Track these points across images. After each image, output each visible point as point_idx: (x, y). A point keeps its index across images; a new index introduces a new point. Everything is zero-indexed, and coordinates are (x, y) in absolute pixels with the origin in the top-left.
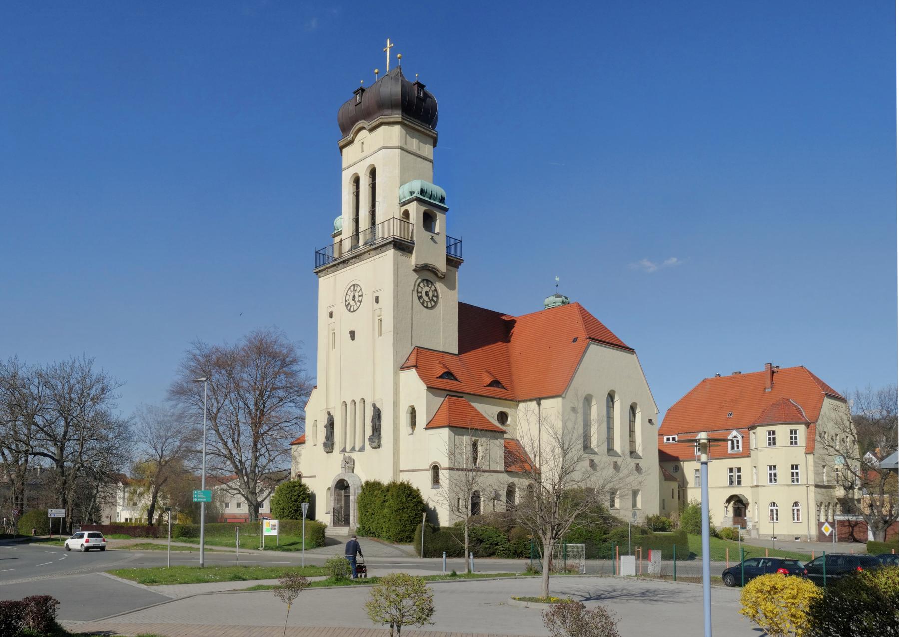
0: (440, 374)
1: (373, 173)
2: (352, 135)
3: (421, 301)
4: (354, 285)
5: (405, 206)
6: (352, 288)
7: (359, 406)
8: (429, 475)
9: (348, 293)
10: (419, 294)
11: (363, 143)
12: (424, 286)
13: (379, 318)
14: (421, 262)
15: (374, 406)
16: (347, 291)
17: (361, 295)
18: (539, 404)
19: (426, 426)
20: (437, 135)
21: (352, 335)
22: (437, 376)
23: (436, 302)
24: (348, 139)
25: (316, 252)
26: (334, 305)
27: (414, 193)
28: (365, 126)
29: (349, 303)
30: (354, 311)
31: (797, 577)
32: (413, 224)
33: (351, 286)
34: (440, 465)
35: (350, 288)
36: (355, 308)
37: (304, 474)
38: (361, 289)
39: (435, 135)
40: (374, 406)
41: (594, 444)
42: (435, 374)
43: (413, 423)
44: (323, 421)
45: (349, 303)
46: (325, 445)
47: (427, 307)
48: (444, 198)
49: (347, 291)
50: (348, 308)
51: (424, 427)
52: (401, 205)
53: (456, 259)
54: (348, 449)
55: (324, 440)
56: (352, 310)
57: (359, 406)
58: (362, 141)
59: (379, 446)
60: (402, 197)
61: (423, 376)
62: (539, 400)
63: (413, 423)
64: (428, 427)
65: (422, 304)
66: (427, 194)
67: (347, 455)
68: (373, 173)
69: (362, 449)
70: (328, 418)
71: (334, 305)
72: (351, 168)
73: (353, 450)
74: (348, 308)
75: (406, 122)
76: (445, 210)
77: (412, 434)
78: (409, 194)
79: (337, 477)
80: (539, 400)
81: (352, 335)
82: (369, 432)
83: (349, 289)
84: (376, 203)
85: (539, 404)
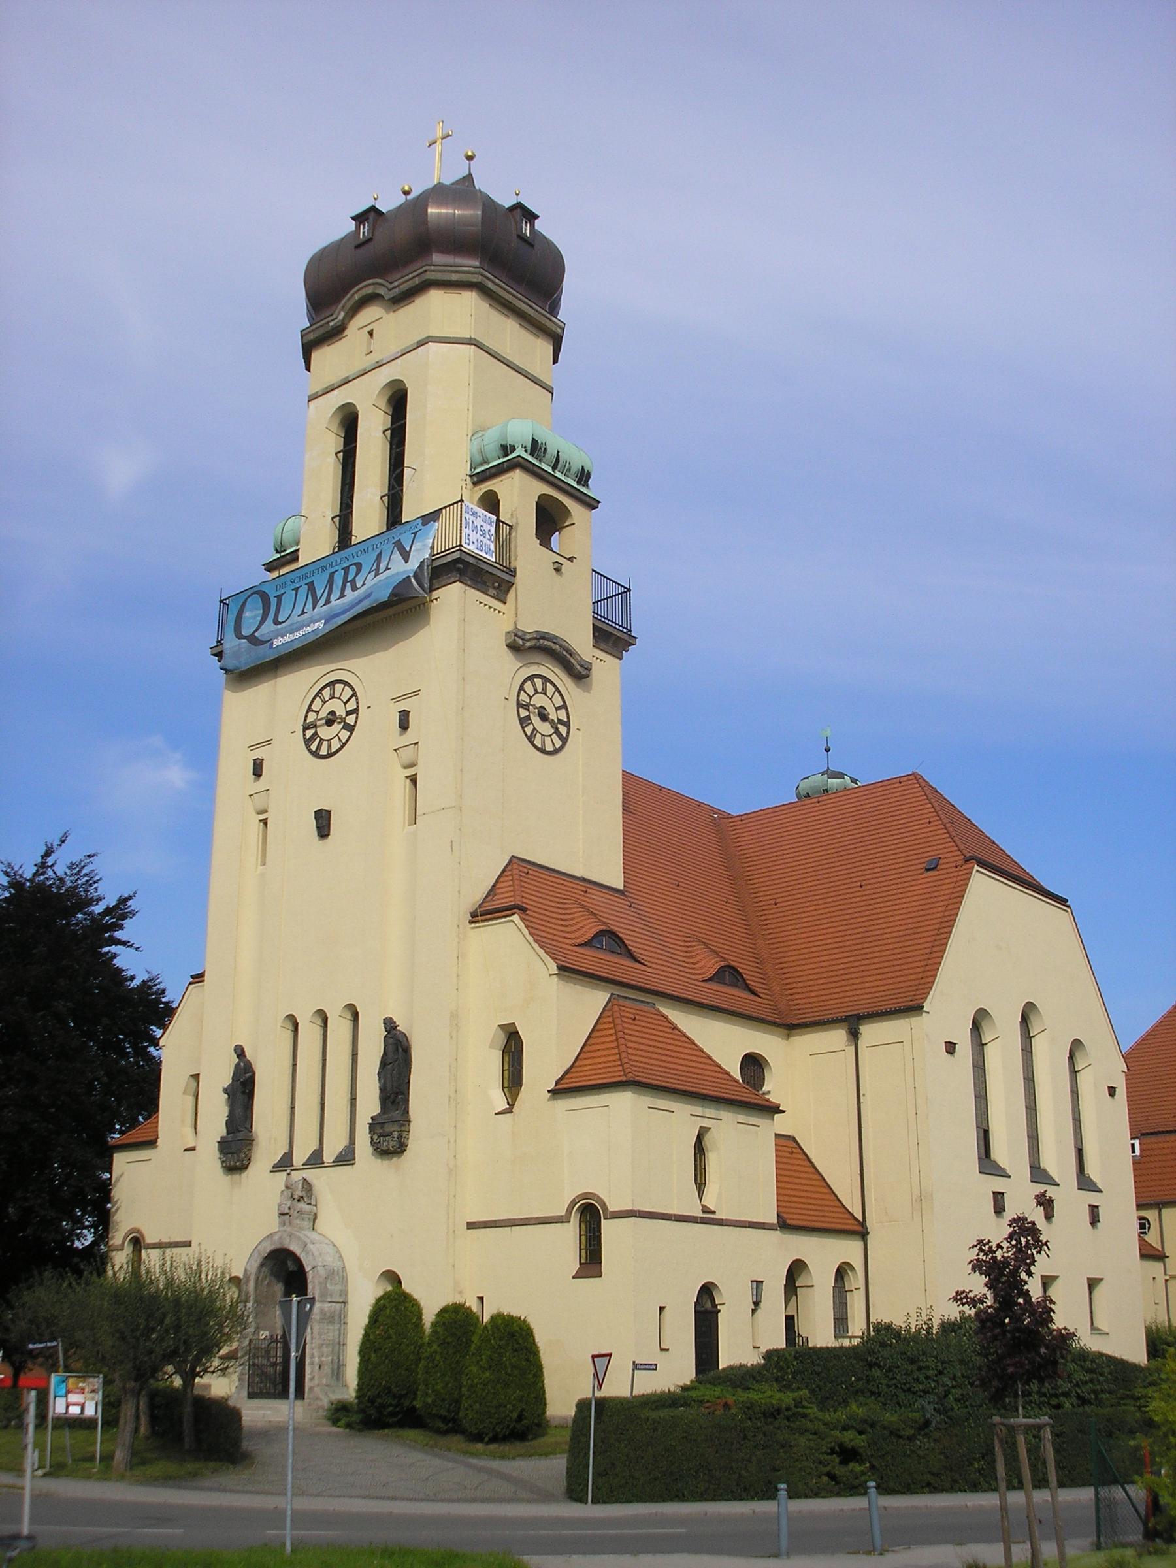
0: (588, 936)
1: (398, 401)
2: (342, 314)
3: (529, 730)
4: (332, 684)
5: (489, 483)
6: (326, 693)
7: (339, 1028)
8: (569, 1235)
9: (315, 707)
10: (524, 713)
11: (371, 333)
12: (536, 692)
13: (410, 772)
14: (530, 626)
15: (390, 1025)
16: (312, 702)
17: (355, 711)
18: (854, 1035)
19: (557, 1083)
20: (563, 329)
21: (323, 823)
22: (579, 941)
23: (564, 740)
24: (332, 324)
25: (221, 601)
26: (268, 742)
27: (513, 449)
28: (381, 291)
29: (316, 733)
30: (330, 755)
31: (1080, 1500)
32: (511, 527)
33: (324, 688)
34: (604, 1205)
35: (320, 692)
36: (335, 745)
37: (150, 1239)
38: (354, 695)
39: (559, 331)
40: (390, 1025)
41: (999, 1153)
42: (572, 936)
43: (513, 1080)
44: (219, 1075)
45: (316, 733)
46: (225, 1146)
47: (542, 750)
48: (589, 474)
49: (312, 702)
50: (313, 747)
51: (552, 1087)
52: (475, 479)
53: (616, 632)
54: (299, 1159)
55: (222, 1131)
56: (323, 751)
57: (339, 1028)
58: (369, 328)
59: (400, 1149)
60: (478, 459)
61: (543, 939)
62: (853, 1024)
63: (513, 1080)
64: (558, 1092)
65: (530, 739)
66: (547, 456)
67: (297, 1176)
68: (398, 401)
69: (346, 1158)
70: (237, 1066)
71: (268, 742)
72: (335, 392)
73: (316, 1160)
74: (313, 747)
75: (490, 285)
76: (591, 504)
77: (509, 1111)
78: (501, 453)
79: (264, 1244)
80: (853, 1024)
81: (323, 823)
82: (370, 1105)
83: (317, 695)
84: (406, 471)
85: (854, 1035)
